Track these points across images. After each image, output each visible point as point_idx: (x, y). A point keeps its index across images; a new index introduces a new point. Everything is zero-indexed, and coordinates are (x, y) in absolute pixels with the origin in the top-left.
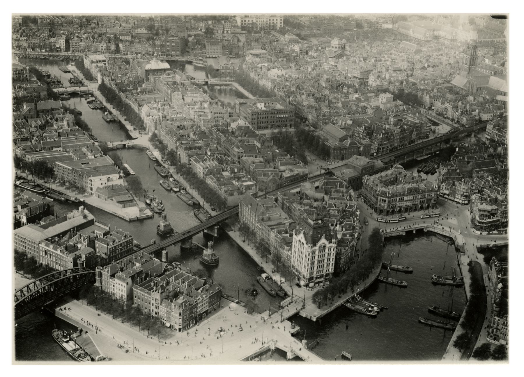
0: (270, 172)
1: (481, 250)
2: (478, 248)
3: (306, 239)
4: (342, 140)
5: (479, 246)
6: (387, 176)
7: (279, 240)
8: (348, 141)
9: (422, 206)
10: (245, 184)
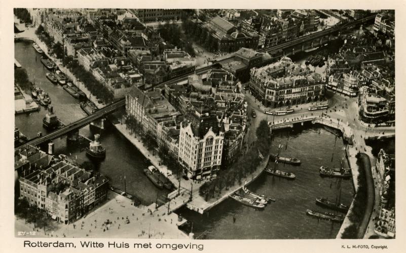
0: (157, 65)
1: (369, 142)
2: (366, 140)
3: (193, 132)
4: (230, 32)
5: (367, 138)
6: (275, 68)
7: (166, 133)
8: (237, 33)
9: (310, 98)
10: (132, 76)
